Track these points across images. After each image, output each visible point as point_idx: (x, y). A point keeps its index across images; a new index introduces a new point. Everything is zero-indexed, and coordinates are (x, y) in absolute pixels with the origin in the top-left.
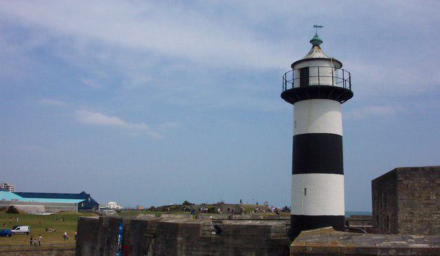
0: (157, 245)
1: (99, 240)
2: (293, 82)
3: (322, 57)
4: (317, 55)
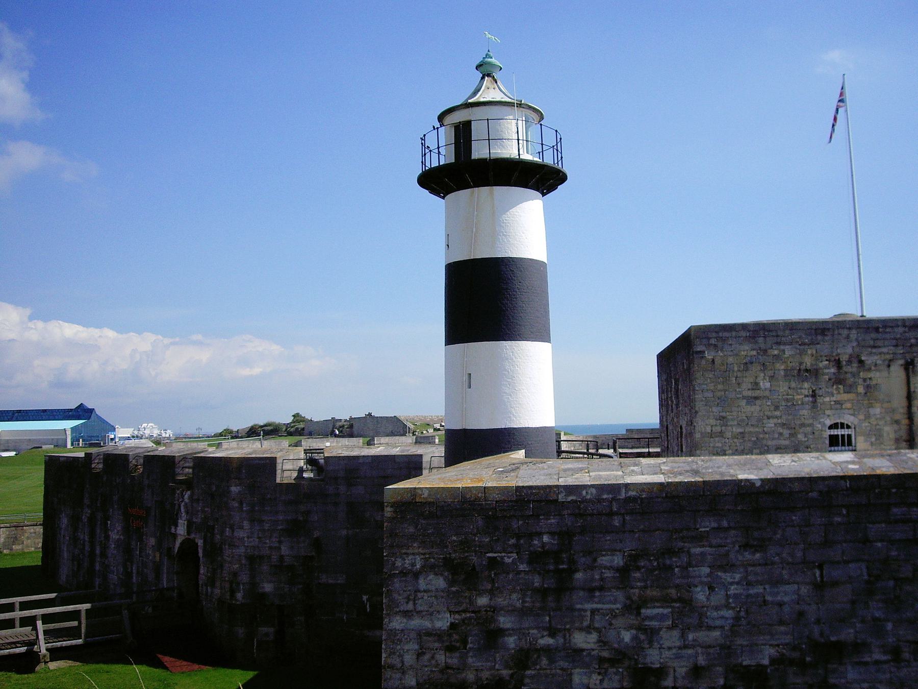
0: (195, 505)
1: (87, 501)
2: (443, 156)
3: (498, 99)
4: (489, 93)
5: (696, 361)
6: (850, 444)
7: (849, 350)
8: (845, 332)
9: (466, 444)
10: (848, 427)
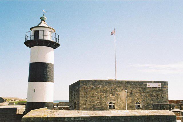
5: (80, 88)
6: (113, 107)
7: (114, 87)
8: (113, 83)
9: (31, 106)
10: (113, 103)
